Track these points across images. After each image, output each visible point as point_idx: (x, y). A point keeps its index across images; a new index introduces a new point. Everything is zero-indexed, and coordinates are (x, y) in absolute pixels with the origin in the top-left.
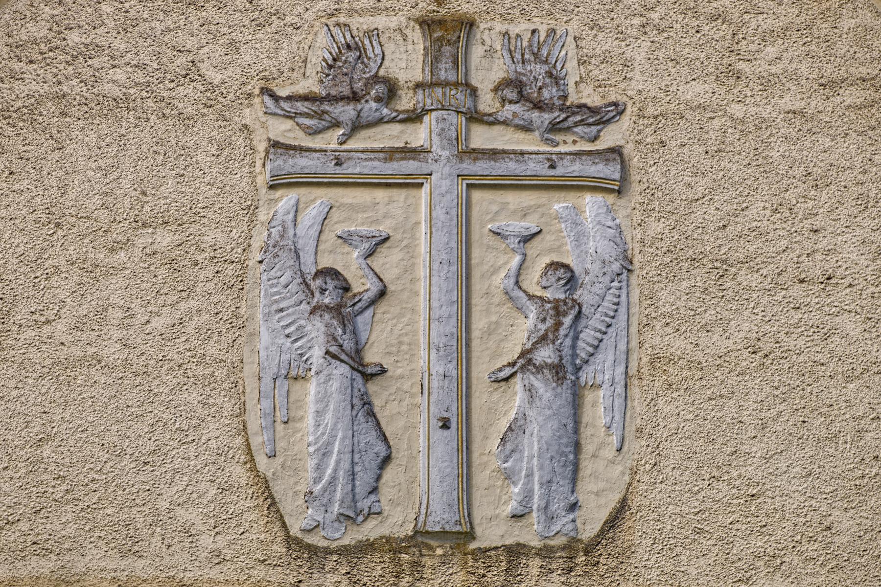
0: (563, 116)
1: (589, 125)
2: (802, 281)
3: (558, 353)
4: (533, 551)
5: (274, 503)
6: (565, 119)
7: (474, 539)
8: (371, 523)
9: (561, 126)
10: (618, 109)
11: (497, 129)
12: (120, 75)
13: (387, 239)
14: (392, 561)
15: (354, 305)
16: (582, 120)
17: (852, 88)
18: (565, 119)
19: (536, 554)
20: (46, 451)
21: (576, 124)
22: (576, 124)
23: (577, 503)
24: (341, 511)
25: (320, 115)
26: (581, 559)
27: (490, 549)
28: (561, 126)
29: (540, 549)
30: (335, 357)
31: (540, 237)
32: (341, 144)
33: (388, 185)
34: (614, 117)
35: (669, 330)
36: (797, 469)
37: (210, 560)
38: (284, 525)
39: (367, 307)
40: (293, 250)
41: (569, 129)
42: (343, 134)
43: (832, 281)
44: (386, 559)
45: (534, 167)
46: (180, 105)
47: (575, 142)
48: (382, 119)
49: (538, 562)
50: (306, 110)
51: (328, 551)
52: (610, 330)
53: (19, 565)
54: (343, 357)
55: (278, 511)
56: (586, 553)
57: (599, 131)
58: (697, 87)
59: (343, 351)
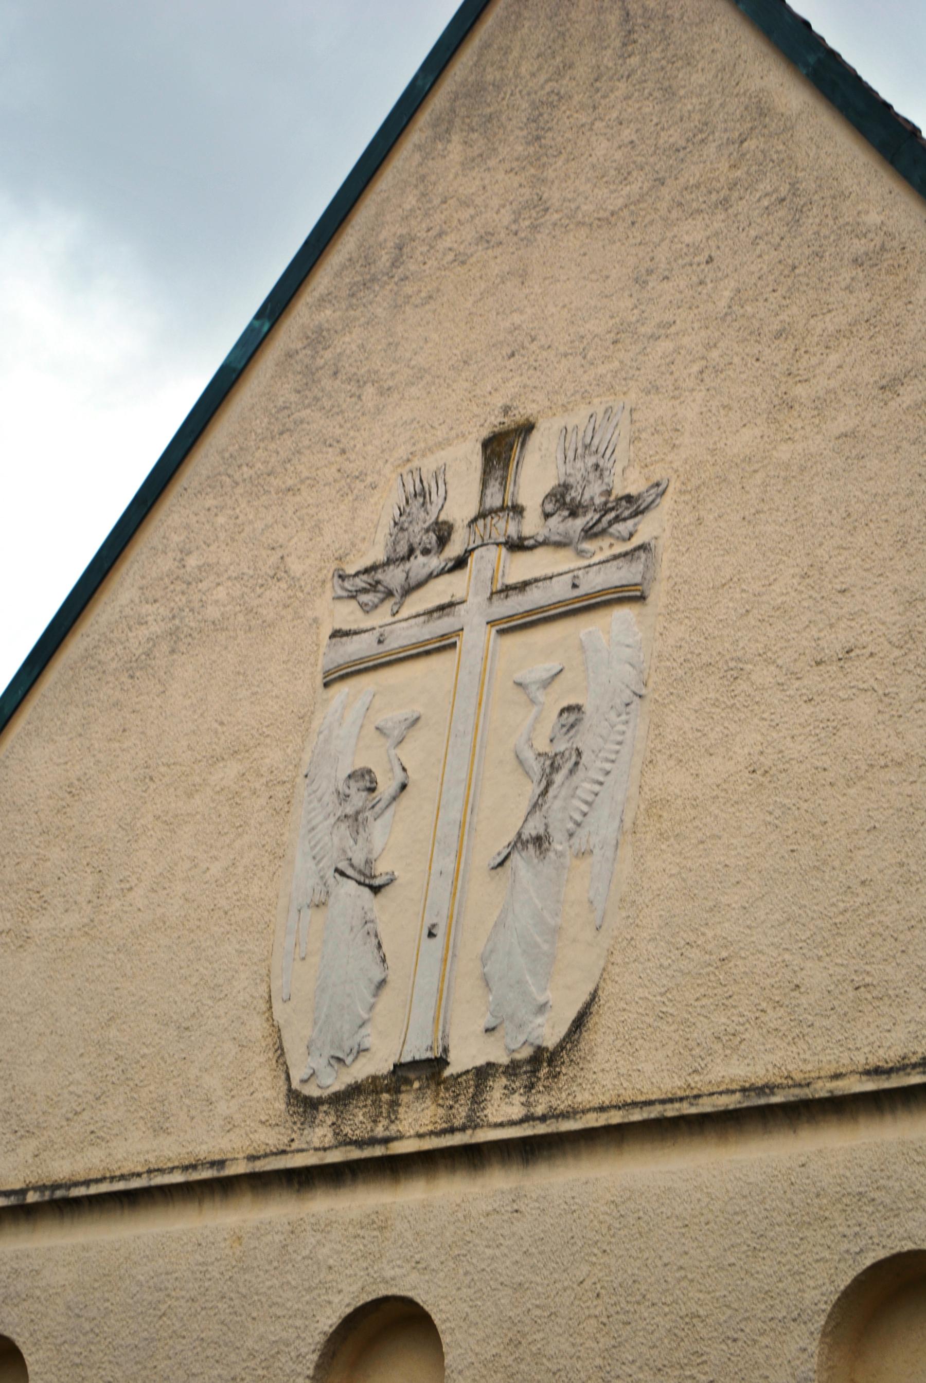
0: (597, 516)
1: (625, 519)
2: (818, 663)
3: (544, 821)
4: (501, 1070)
5: (283, 1054)
6: (599, 520)
7: (448, 1064)
8: (362, 1060)
9: (595, 530)
10: (659, 488)
11: (540, 552)
12: (221, 593)
13: (418, 719)
14: (374, 1102)
15: (373, 807)
16: (617, 517)
17: (916, 381)
18: (599, 520)
19: (503, 1073)
20: (113, 1032)
21: (610, 524)
22: (610, 524)
23: (547, 1003)
24: (332, 1053)
25: (374, 587)
26: (544, 1070)
27: (459, 1076)
28: (595, 530)
29: (508, 1067)
30: (342, 874)
31: (562, 676)
32: (394, 615)
33: (428, 653)
34: (653, 502)
35: (672, 763)
36: (777, 916)
37: (222, 1127)
38: (288, 1078)
39: (387, 806)
40: (858, 693)
41: (604, 532)
42: (395, 604)
43: (852, 654)
44: (369, 1102)
45: (559, 590)
46: (265, 612)
47: (611, 545)
48: (431, 574)
49: (504, 1081)
50: (364, 585)
51: (320, 1101)
52: (608, 780)
53: (78, 1157)
54: (350, 872)
55: (285, 1063)
56: (550, 1062)
57: (635, 525)
58: (747, 434)
59: (352, 866)
